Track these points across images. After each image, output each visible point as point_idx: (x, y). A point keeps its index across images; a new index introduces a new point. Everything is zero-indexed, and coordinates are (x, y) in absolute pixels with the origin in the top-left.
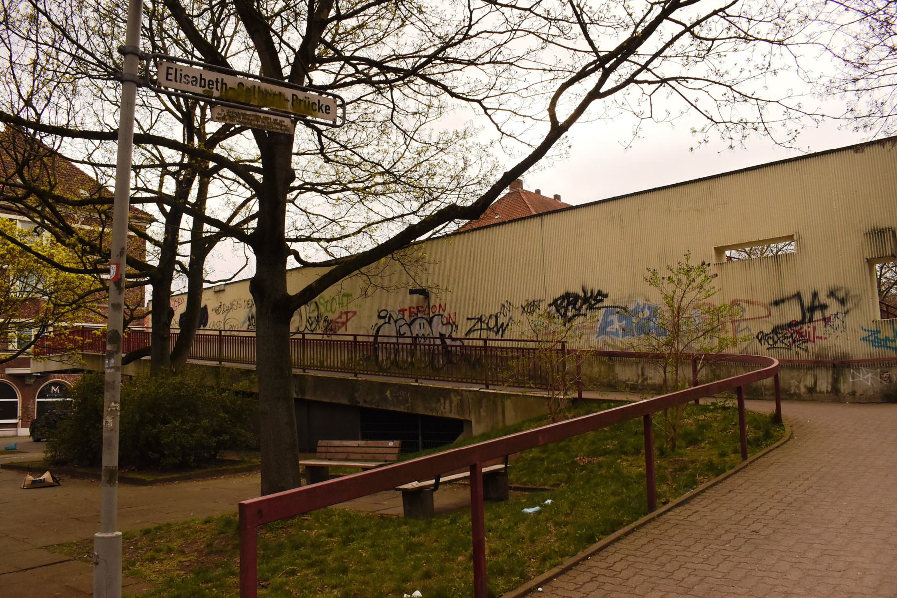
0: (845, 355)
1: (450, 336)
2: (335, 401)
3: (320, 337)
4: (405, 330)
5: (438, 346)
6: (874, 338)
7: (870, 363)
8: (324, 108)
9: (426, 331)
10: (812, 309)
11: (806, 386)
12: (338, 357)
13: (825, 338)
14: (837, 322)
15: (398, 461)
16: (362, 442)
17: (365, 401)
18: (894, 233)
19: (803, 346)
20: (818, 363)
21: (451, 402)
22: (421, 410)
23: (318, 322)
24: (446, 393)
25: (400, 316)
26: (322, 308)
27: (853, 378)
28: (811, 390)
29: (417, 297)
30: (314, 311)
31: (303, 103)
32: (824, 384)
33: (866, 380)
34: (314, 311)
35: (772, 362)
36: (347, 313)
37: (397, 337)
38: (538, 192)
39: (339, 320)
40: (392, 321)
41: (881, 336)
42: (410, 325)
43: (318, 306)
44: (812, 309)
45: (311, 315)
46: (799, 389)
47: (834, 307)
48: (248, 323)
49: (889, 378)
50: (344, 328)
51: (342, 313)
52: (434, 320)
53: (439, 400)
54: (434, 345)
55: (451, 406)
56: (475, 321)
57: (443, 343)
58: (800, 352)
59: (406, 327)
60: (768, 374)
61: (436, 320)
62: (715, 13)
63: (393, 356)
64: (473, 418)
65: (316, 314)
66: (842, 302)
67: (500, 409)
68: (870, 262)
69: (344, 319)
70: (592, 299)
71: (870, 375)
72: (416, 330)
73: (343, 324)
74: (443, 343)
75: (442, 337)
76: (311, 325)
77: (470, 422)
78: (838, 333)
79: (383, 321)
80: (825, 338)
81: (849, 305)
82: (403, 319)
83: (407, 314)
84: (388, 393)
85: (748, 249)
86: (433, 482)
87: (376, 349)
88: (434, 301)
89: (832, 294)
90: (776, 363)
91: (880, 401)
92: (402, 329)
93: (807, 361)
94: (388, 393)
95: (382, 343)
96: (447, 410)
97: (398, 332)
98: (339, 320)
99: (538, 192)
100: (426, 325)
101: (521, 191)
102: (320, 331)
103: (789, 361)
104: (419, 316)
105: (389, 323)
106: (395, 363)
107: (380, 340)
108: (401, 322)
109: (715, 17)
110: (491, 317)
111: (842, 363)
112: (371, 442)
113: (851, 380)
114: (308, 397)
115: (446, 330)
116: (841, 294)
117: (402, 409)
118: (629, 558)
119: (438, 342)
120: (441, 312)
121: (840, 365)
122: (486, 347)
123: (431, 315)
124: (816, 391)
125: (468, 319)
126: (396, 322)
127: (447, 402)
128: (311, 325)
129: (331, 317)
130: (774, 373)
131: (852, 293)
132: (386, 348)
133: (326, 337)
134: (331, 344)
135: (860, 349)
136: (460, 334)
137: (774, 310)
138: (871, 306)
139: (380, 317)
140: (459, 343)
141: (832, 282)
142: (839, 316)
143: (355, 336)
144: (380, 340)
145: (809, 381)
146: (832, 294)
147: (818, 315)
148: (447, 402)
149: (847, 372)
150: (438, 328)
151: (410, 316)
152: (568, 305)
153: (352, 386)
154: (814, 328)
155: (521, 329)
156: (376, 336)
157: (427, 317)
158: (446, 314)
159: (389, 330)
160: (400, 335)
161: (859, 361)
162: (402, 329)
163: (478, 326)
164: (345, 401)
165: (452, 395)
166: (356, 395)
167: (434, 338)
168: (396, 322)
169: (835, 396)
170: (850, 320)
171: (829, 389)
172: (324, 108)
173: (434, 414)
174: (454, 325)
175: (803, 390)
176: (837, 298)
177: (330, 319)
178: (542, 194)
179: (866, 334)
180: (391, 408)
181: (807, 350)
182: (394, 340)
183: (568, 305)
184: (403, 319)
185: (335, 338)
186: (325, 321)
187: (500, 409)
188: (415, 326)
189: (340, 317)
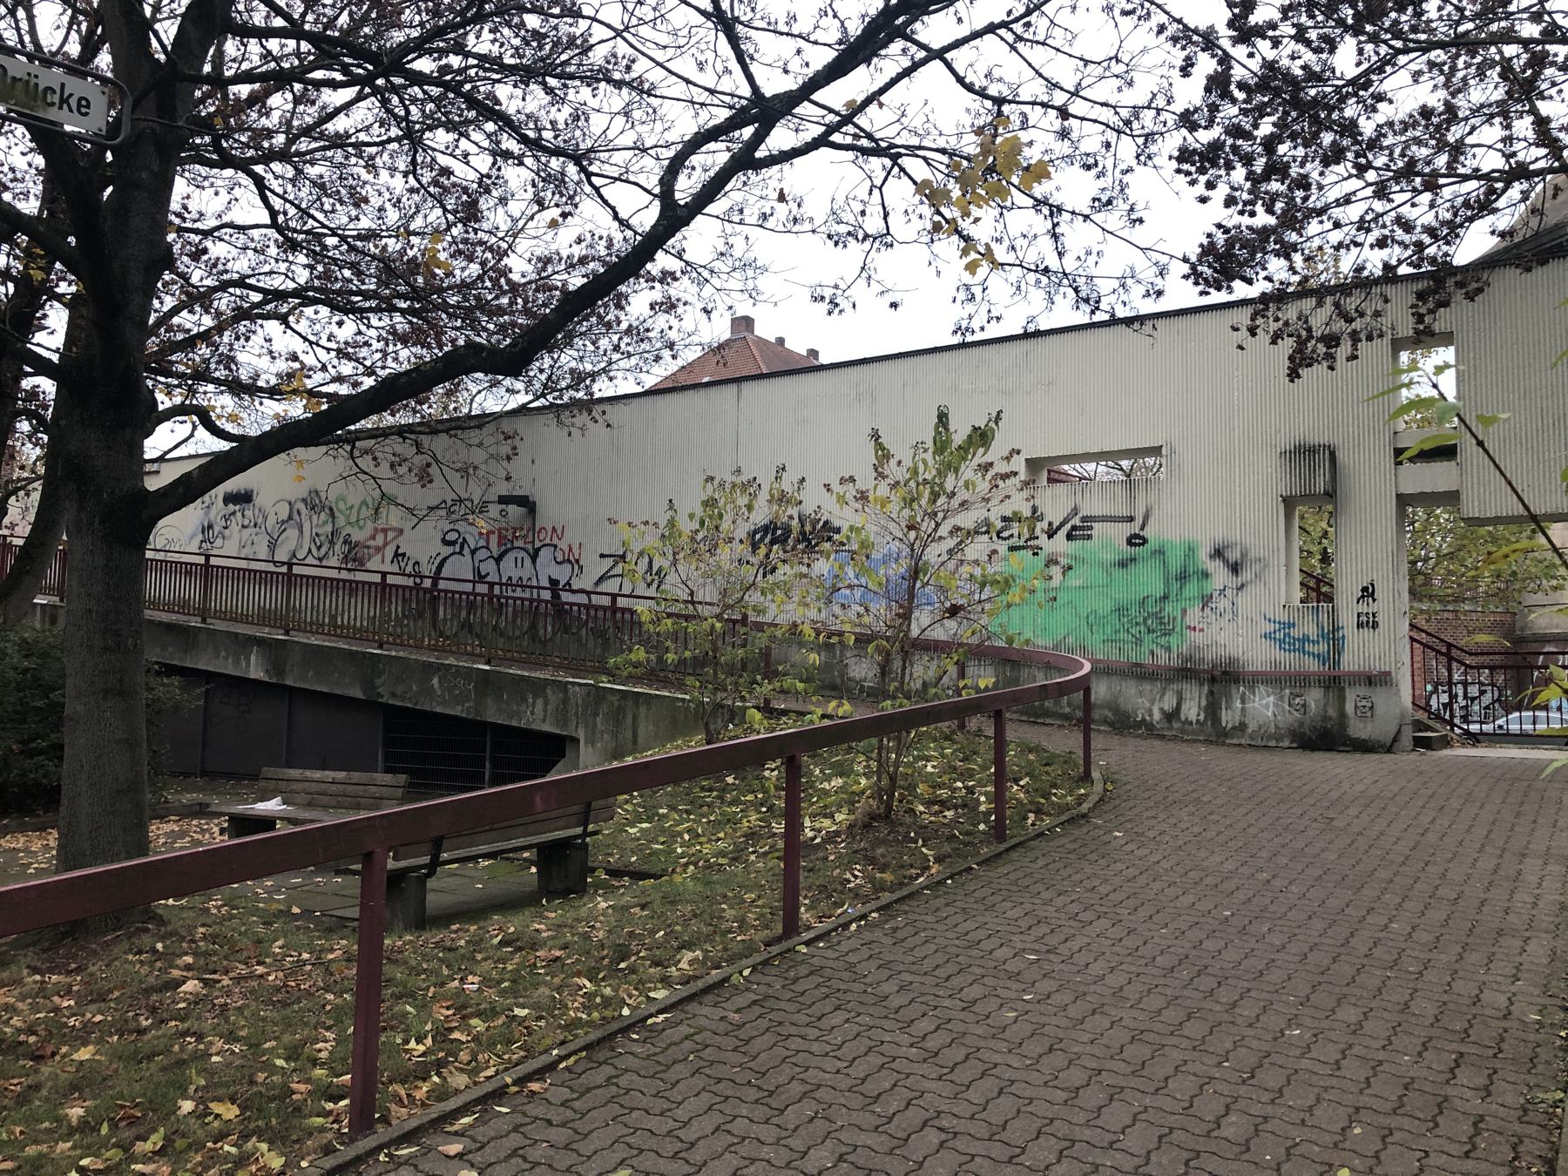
0: (1232, 661)
1: (568, 583)
2: (338, 692)
3: (333, 574)
4: (489, 567)
5: (547, 602)
6: (1283, 636)
7: (1275, 679)
8: (73, 102)
9: (526, 571)
10: (1183, 577)
11: (1162, 709)
12: (359, 612)
13: (1202, 630)
14: (1223, 604)
15: (57, 872)
16: (341, 775)
17: (393, 695)
18: (1333, 455)
19: (1163, 641)
20: (1186, 672)
21: (546, 704)
22: (493, 716)
23: (332, 543)
24: (539, 687)
25: (482, 543)
26: (341, 521)
27: (1243, 702)
28: (1171, 716)
29: (513, 510)
30: (325, 523)
31: (19, 85)
32: (1192, 710)
33: (1264, 707)
34: (325, 523)
35: (1082, 666)
36: (385, 531)
37: (474, 582)
38: (781, 341)
39: (372, 543)
40: (466, 551)
41: (1295, 633)
42: (498, 560)
43: (332, 515)
44: (1183, 577)
45: (320, 531)
46: (1151, 715)
47: (1220, 576)
48: (200, 537)
49: (1304, 706)
50: (379, 556)
51: (376, 530)
52: (541, 553)
53: (524, 700)
54: (539, 601)
55: (545, 711)
56: (610, 561)
57: (556, 596)
58: (1158, 651)
59: (491, 564)
60: (1063, 689)
61: (545, 554)
62: (991, 29)
63: (464, 613)
64: (581, 735)
65: (329, 528)
66: (1235, 568)
67: (629, 721)
68: (1289, 503)
69: (380, 540)
70: (815, 536)
71: (1272, 699)
72: (509, 568)
73: (378, 549)
74: (556, 596)
75: (554, 583)
76: (319, 548)
77: (576, 741)
78: (1223, 622)
79: (450, 550)
80: (1202, 630)
81: (1246, 575)
82: (487, 548)
83: (494, 539)
84: (435, 681)
85: (1125, 464)
86: (426, 859)
87: (435, 599)
88: (545, 519)
89: (1218, 553)
90: (1087, 667)
91: (1286, 743)
92: (482, 566)
93: (1169, 669)
94: (435, 681)
95: (446, 592)
96: (538, 718)
97: (476, 571)
98: (372, 543)
99: (781, 341)
100: (528, 561)
101: (749, 337)
102: (333, 562)
103: (1137, 665)
104: (516, 544)
105: (460, 553)
106: (467, 626)
107: (442, 585)
108: (482, 554)
109: (989, 37)
110: (641, 554)
111: (1225, 673)
112: (356, 776)
113: (1238, 704)
114: (289, 682)
115: (562, 574)
116: (1233, 555)
117: (457, 711)
118: (808, 1019)
119: (546, 595)
120: (555, 541)
121: (1223, 678)
122: (614, 608)
123: (538, 544)
124: (1179, 719)
125: (602, 556)
126: (473, 552)
127: (540, 702)
128: (319, 548)
129: (358, 536)
130: (1084, 685)
131: (1252, 554)
132: (453, 598)
133: (344, 575)
134: (353, 587)
135: (1258, 654)
136: (585, 582)
137: (1118, 573)
138: (1283, 574)
139: (446, 542)
140: (582, 599)
141: (1220, 534)
142: (1228, 592)
143: (384, 575)
144: (442, 585)
145: (1169, 703)
146: (1218, 553)
147: (1192, 589)
148: (540, 702)
149: (1234, 691)
150: (548, 568)
151: (499, 545)
152: (772, 543)
153: (368, 666)
154: (1184, 612)
155: (696, 582)
156: (436, 578)
157: (530, 547)
158: (563, 545)
159: (460, 567)
160: (480, 578)
161: (1254, 674)
162: (482, 566)
163: (618, 570)
164: (358, 693)
165: (549, 691)
166: (378, 682)
167: (539, 588)
168: (473, 552)
169: (1216, 733)
170: (1243, 600)
171: (1202, 717)
172: (73, 102)
173: (514, 723)
174: (575, 563)
175: (1157, 716)
176: (1225, 561)
177: (354, 539)
178: (787, 345)
179: (1270, 628)
180: (438, 710)
181: (1168, 649)
182: (468, 587)
183: (772, 543)
184: (487, 548)
185: (360, 576)
186: (345, 542)
187: (629, 721)
188: (508, 565)
189: (373, 538)
